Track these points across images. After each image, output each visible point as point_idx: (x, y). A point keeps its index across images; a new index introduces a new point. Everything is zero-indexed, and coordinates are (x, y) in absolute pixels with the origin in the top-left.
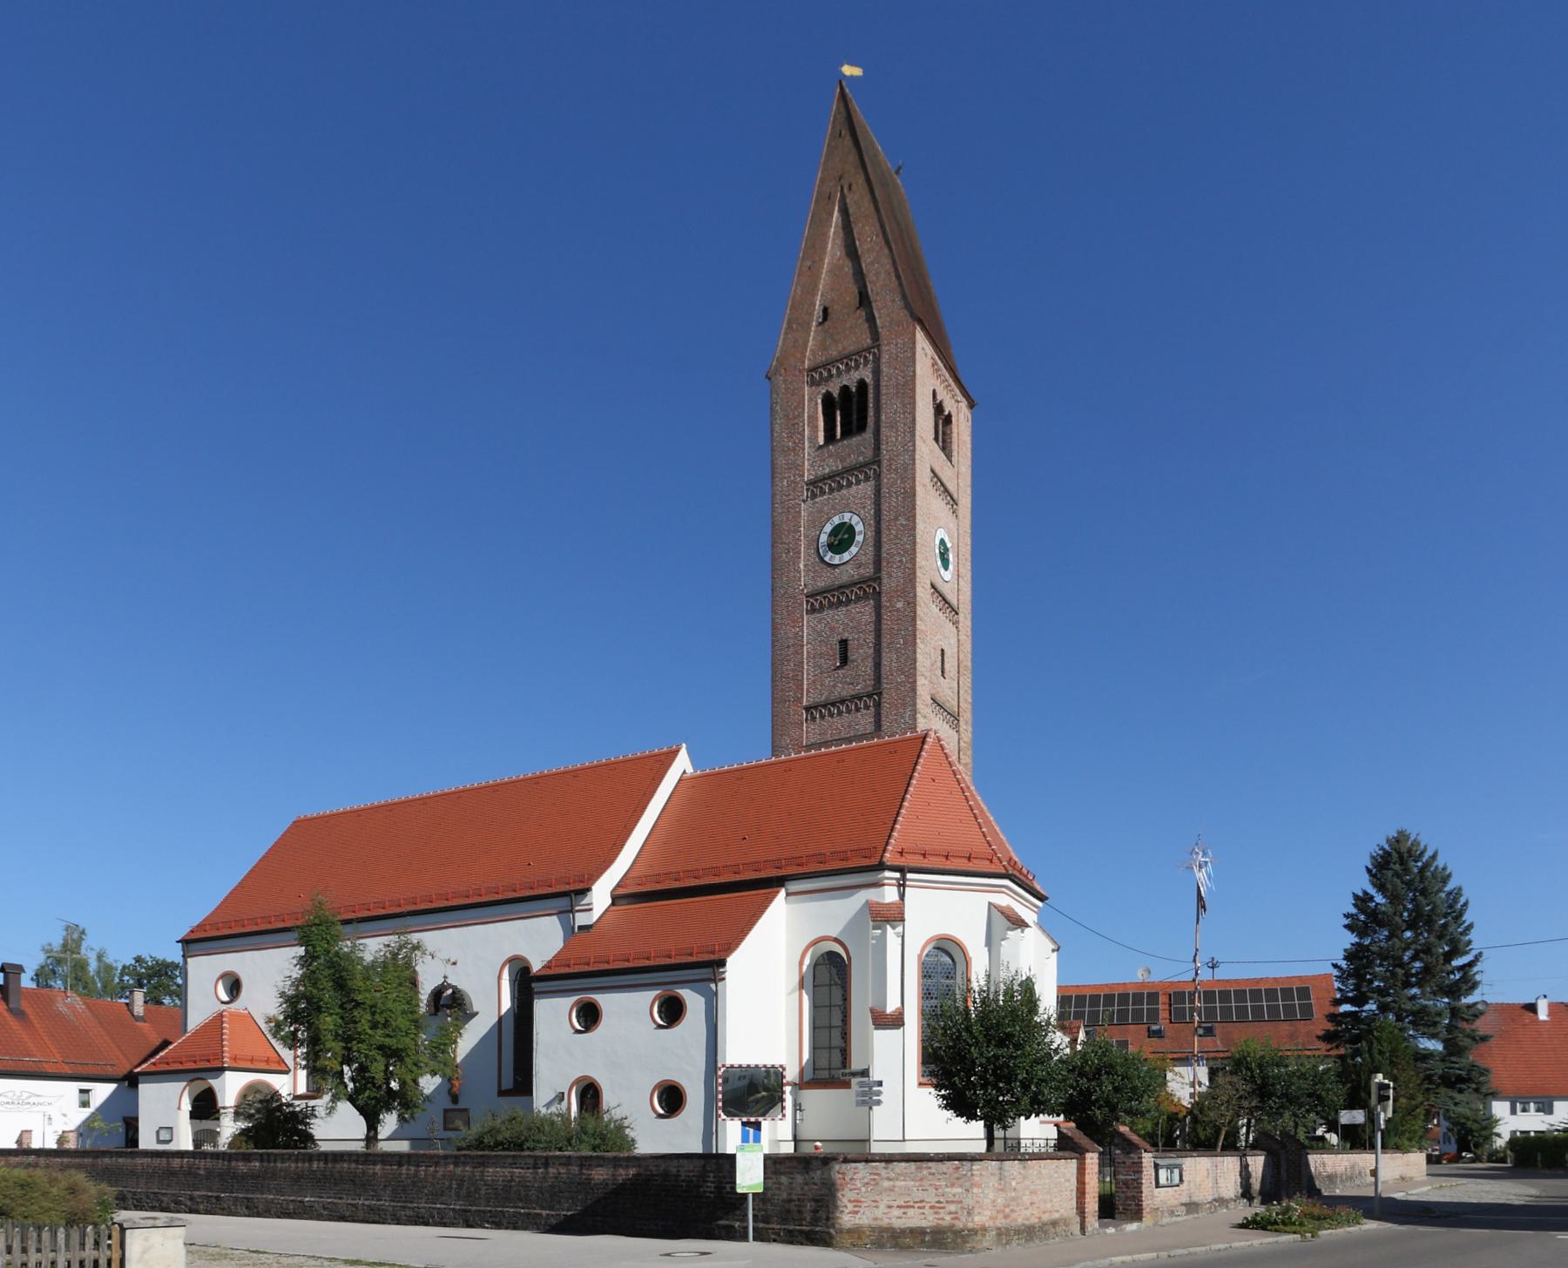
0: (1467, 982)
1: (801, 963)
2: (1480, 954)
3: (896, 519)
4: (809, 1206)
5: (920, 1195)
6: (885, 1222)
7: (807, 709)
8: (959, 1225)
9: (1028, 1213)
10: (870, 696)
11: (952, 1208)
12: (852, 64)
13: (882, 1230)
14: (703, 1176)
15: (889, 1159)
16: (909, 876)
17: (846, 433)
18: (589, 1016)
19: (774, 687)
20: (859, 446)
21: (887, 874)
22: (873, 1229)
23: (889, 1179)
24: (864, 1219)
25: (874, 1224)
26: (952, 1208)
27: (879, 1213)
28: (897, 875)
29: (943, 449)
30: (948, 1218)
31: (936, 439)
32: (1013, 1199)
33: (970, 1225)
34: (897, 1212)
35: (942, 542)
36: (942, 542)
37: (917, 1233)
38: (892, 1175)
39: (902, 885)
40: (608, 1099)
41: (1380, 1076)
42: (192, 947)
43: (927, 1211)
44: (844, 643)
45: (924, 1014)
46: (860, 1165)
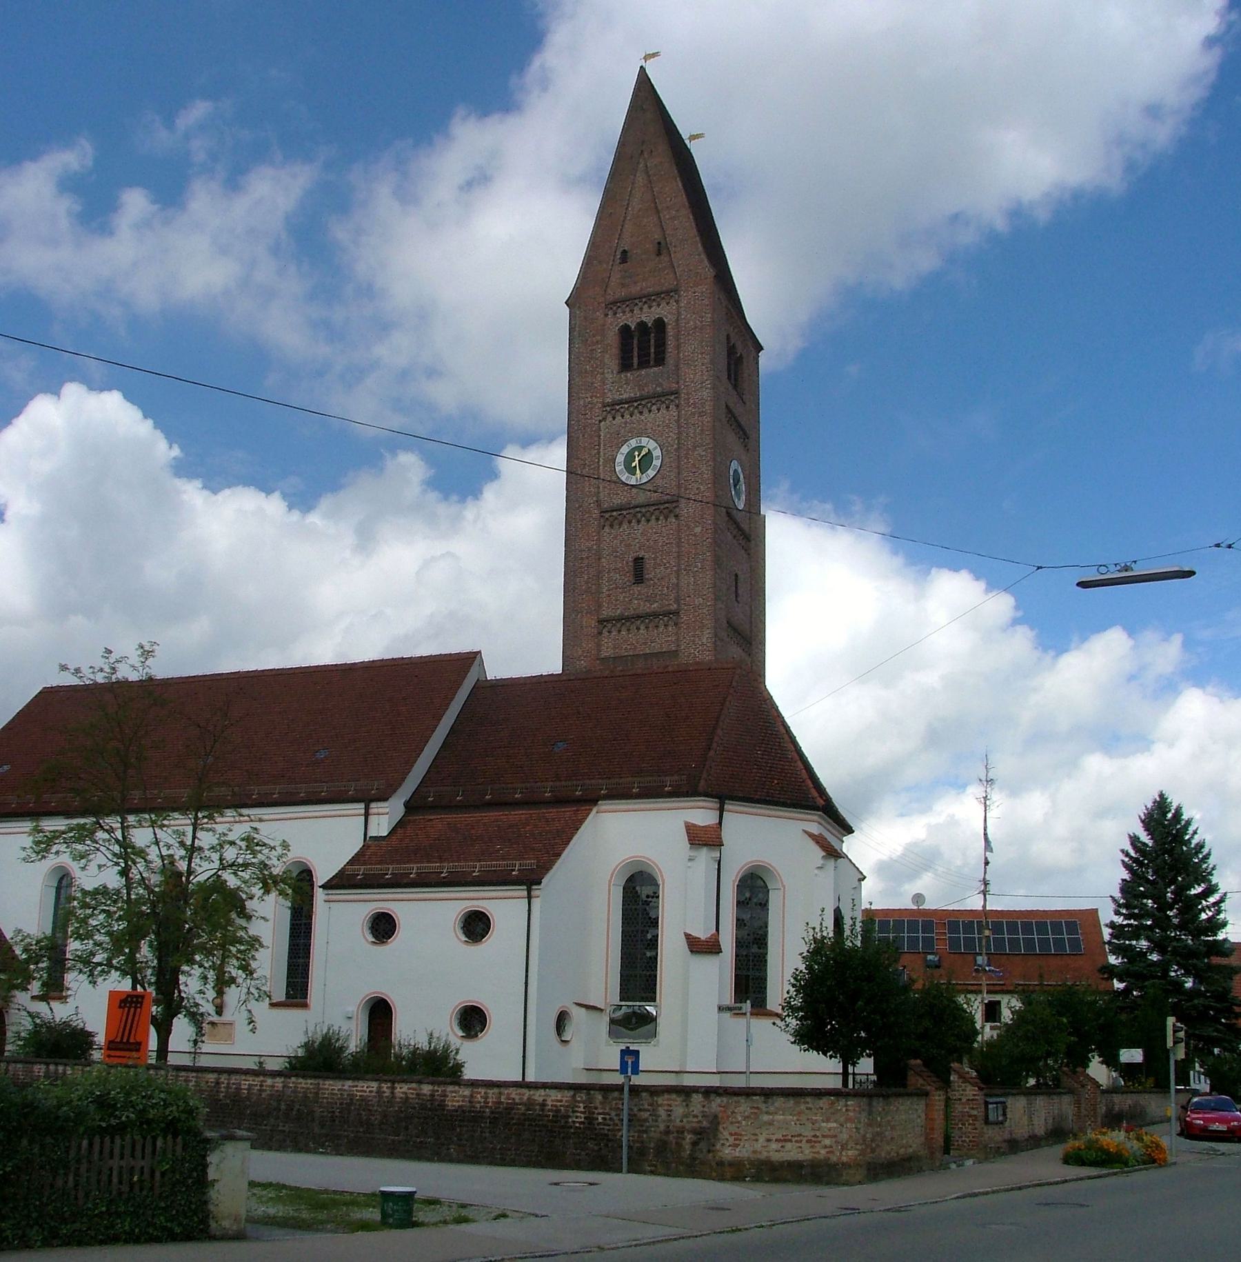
0: (1215, 925)
2: (1225, 894)
4: (689, 1137)
8: (834, 1159)
9: (888, 1148)
11: (827, 1142)
14: (573, 1106)
17: (644, 364)
18: (383, 927)
22: (752, 1163)
23: (767, 1113)
24: (744, 1152)
25: (753, 1157)
26: (827, 1142)
27: (758, 1146)
29: (735, 387)
30: (823, 1152)
31: (729, 378)
32: (878, 1134)
33: (844, 1159)
34: (774, 1146)
35: (735, 471)
36: (735, 471)
38: (772, 1109)
41: (1017, 1004)
43: (804, 1144)
44: (638, 561)
45: (740, 944)
46: (742, 1099)
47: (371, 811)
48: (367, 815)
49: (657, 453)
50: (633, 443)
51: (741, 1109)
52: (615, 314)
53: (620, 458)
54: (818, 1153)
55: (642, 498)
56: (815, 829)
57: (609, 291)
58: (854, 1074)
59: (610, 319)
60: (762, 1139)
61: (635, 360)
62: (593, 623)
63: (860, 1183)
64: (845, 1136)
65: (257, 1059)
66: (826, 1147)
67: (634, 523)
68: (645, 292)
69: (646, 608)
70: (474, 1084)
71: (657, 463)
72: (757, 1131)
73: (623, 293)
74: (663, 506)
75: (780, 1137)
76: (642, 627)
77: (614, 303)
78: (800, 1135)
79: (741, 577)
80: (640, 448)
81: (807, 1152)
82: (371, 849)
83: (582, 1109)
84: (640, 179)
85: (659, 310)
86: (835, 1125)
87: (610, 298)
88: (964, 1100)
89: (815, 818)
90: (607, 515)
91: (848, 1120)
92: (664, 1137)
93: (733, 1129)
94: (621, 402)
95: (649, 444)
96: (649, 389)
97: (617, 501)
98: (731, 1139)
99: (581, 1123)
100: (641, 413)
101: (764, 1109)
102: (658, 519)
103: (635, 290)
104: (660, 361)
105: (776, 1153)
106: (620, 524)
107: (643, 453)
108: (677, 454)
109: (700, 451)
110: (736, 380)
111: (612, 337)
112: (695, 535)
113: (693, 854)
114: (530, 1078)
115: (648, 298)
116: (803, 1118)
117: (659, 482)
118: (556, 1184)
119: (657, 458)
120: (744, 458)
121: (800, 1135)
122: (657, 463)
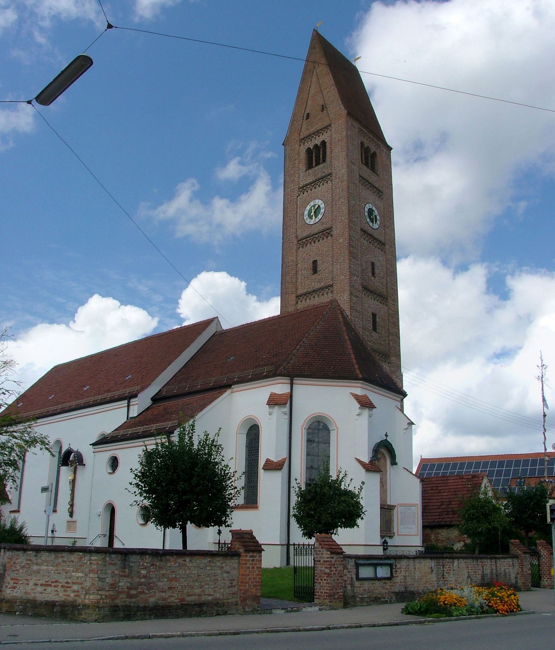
5: (56, 577)
6: (31, 597)
8: (79, 601)
11: (75, 587)
13: (29, 601)
15: (38, 549)
17: (318, 164)
20: (319, 170)
23: (37, 564)
26: (75, 587)
27: (29, 589)
30: (72, 595)
33: (87, 601)
34: (39, 589)
37: (51, 605)
40: (45, 485)
43: (59, 589)
44: (315, 262)
47: (131, 404)
48: (128, 406)
49: (322, 206)
50: (312, 204)
52: (304, 144)
53: (306, 212)
54: (69, 596)
55: (316, 231)
56: (359, 392)
57: (301, 134)
59: (301, 148)
60: (31, 584)
61: (314, 163)
62: (294, 298)
63: (96, 621)
64: (88, 584)
65: (73, 540)
66: (74, 591)
67: (313, 243)
69: (318, 286)
71: (322, 211)
72: (29, 578)
73: (307, 133)
74: (326, 232)
75: (44, 582)
76: (316, 296)
77: (303, 139)
78: (57, 581)
79: (377, 264)
80: (314, 206)
82: (131, 422)
84: (314, 79)
85: (323, 137)
86: (81, 574)
87: (302, 137)
88: (322, 562)
89: (359, 385)
90: (300, 242)
91: (91, 571)
93: (14, 575)
94: (307, 185)
95: (319, 202)
96: (319, 176)
97: (305, 234)
98: (12, 582)
100: (315, 188)
101: (35, 561)
102: (323, 239)
103: (312, 130)
104: (324, 161)
106: (306, 245)
107: (316, 207)
108: (331, 204)
109: (342, 200)
111: (303, 155)
112: (340, 243)
113: (271, 410)
114: (167, 547)
115: (317, 133)
116: (60, 568)
117: (323, 220)
121: (57, 581)
122: (322, 211)
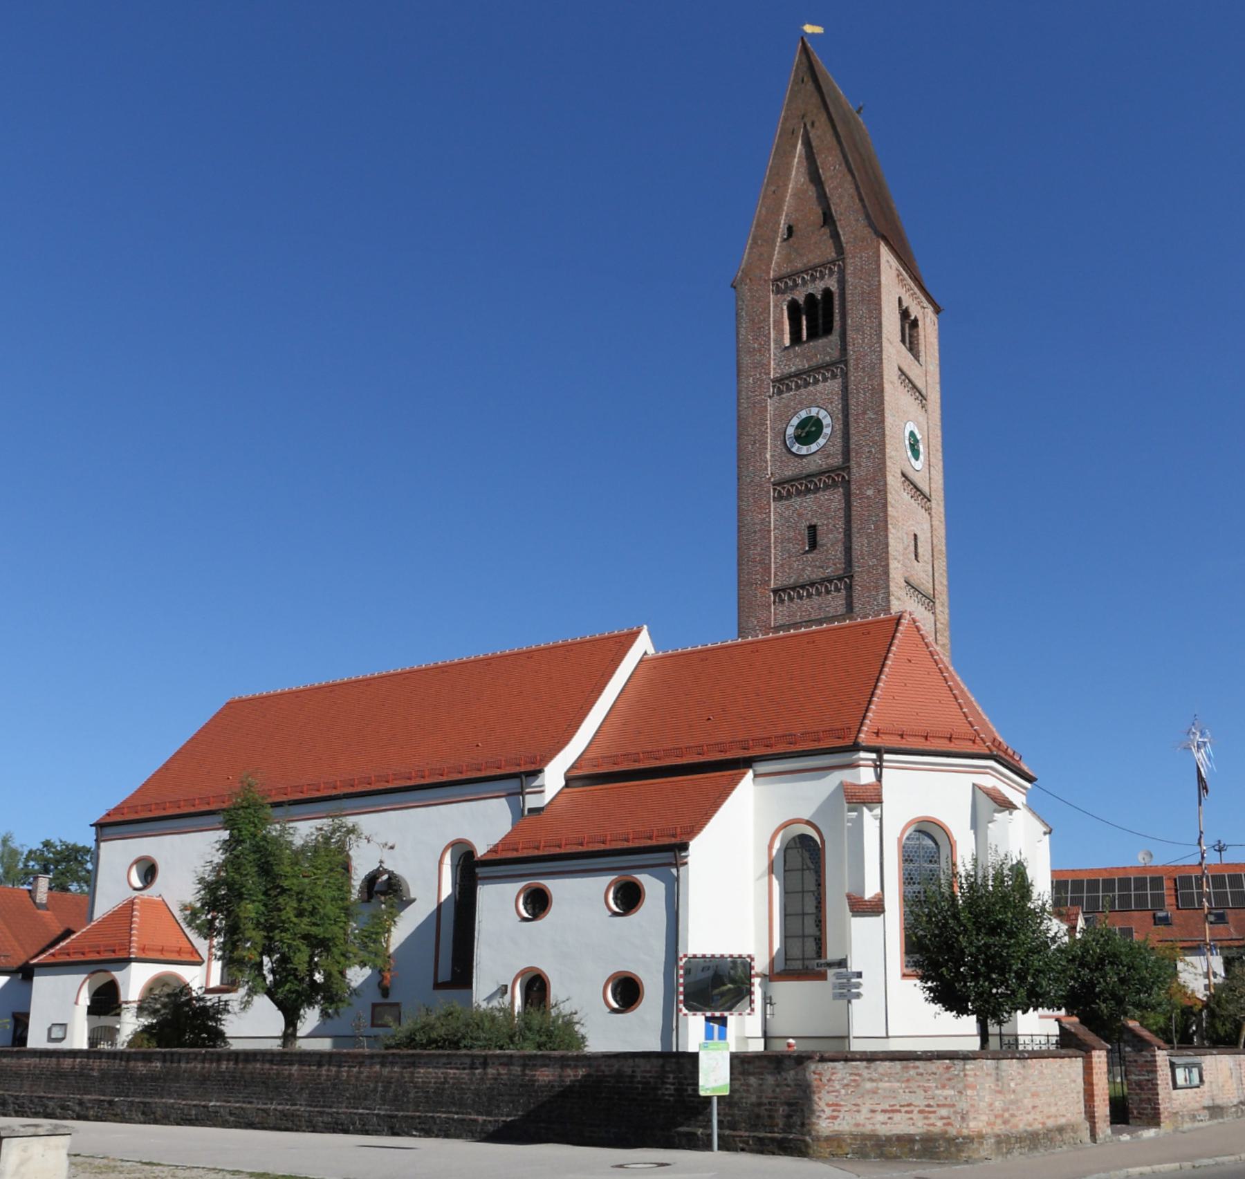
1: (770, 847)
3: (864, 413)
4: (782, 1110)
7: (775, 591)
8: (952, 1131)
10: (840, 579)
11: (944, 1112)
12: (813, 23)
16: (886, 757)
17: (813, 335)
18: (538, 903)
19: (740, 571)
21: (863, 755)
22: (854, 1137)
23: (871, 1080)
25: (855, 1130)
26: (944, 1112)
27: (861, 1118)
28: (874, 756)
29: (911, 350)
30: (940, 1124)
31: (903, 341)
32: (1012, 1102)
34: (881, 1117)
38: (875, 1076)
39: (878, 766)
42: (107, 830)
43: (915, 1115)
44: (813, 529)
46: (839, 1065)
51: (839, 1076)
58: (1001, 1035)
66: (942, 1118)
68: (811, 264)
70: (237, 1056)
72: (859, 1101)
78: (909, 1105)
81: (920, 1124)
83: (671, 1080)
86: (952, 1092)
92: (756, 1110)
93: (830, 1098)
99: (671, 1095)
105: (884, 1126)
110: (911, 343)
116: (913, 1085)
118: (621, 1166)
119: (828, 426)
120: (921, 419)
121: (909, 1105)
